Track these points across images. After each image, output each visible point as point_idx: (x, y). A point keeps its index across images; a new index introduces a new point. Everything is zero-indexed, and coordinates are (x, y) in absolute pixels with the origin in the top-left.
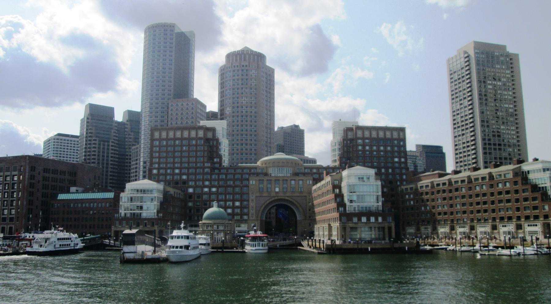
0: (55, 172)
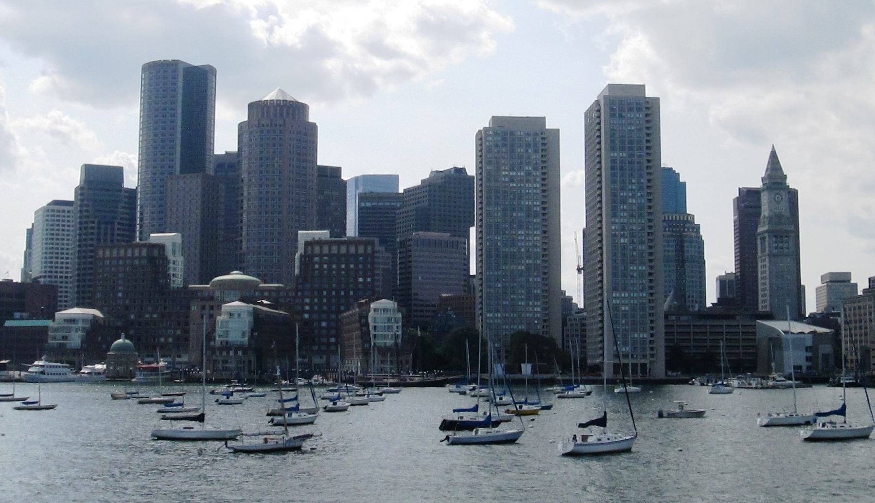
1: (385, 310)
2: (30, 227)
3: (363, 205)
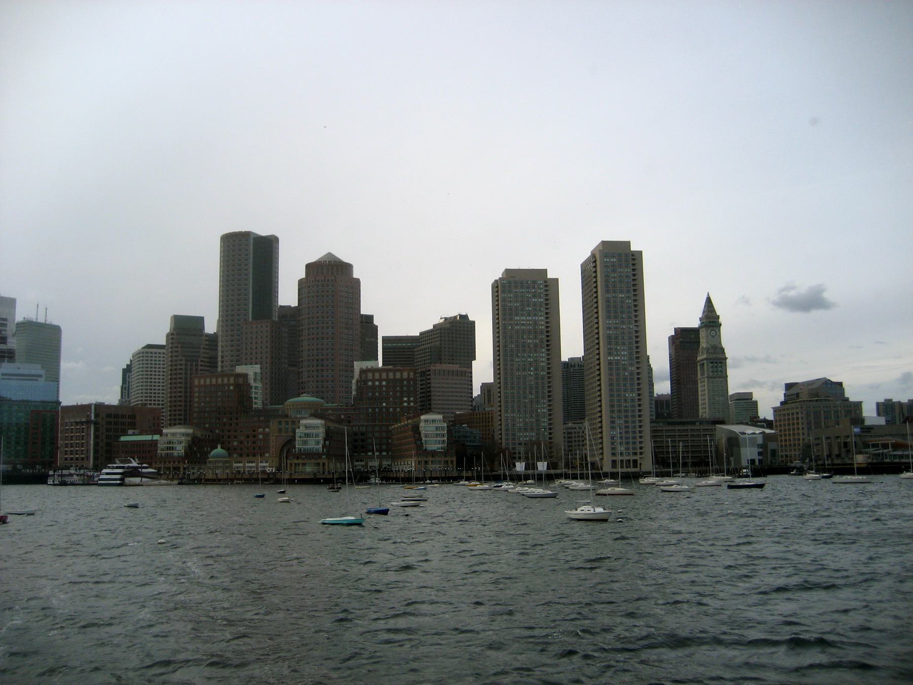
0: (116, 416)
1: (434, 421)
2: (129, 363)
3: (385, 345)
